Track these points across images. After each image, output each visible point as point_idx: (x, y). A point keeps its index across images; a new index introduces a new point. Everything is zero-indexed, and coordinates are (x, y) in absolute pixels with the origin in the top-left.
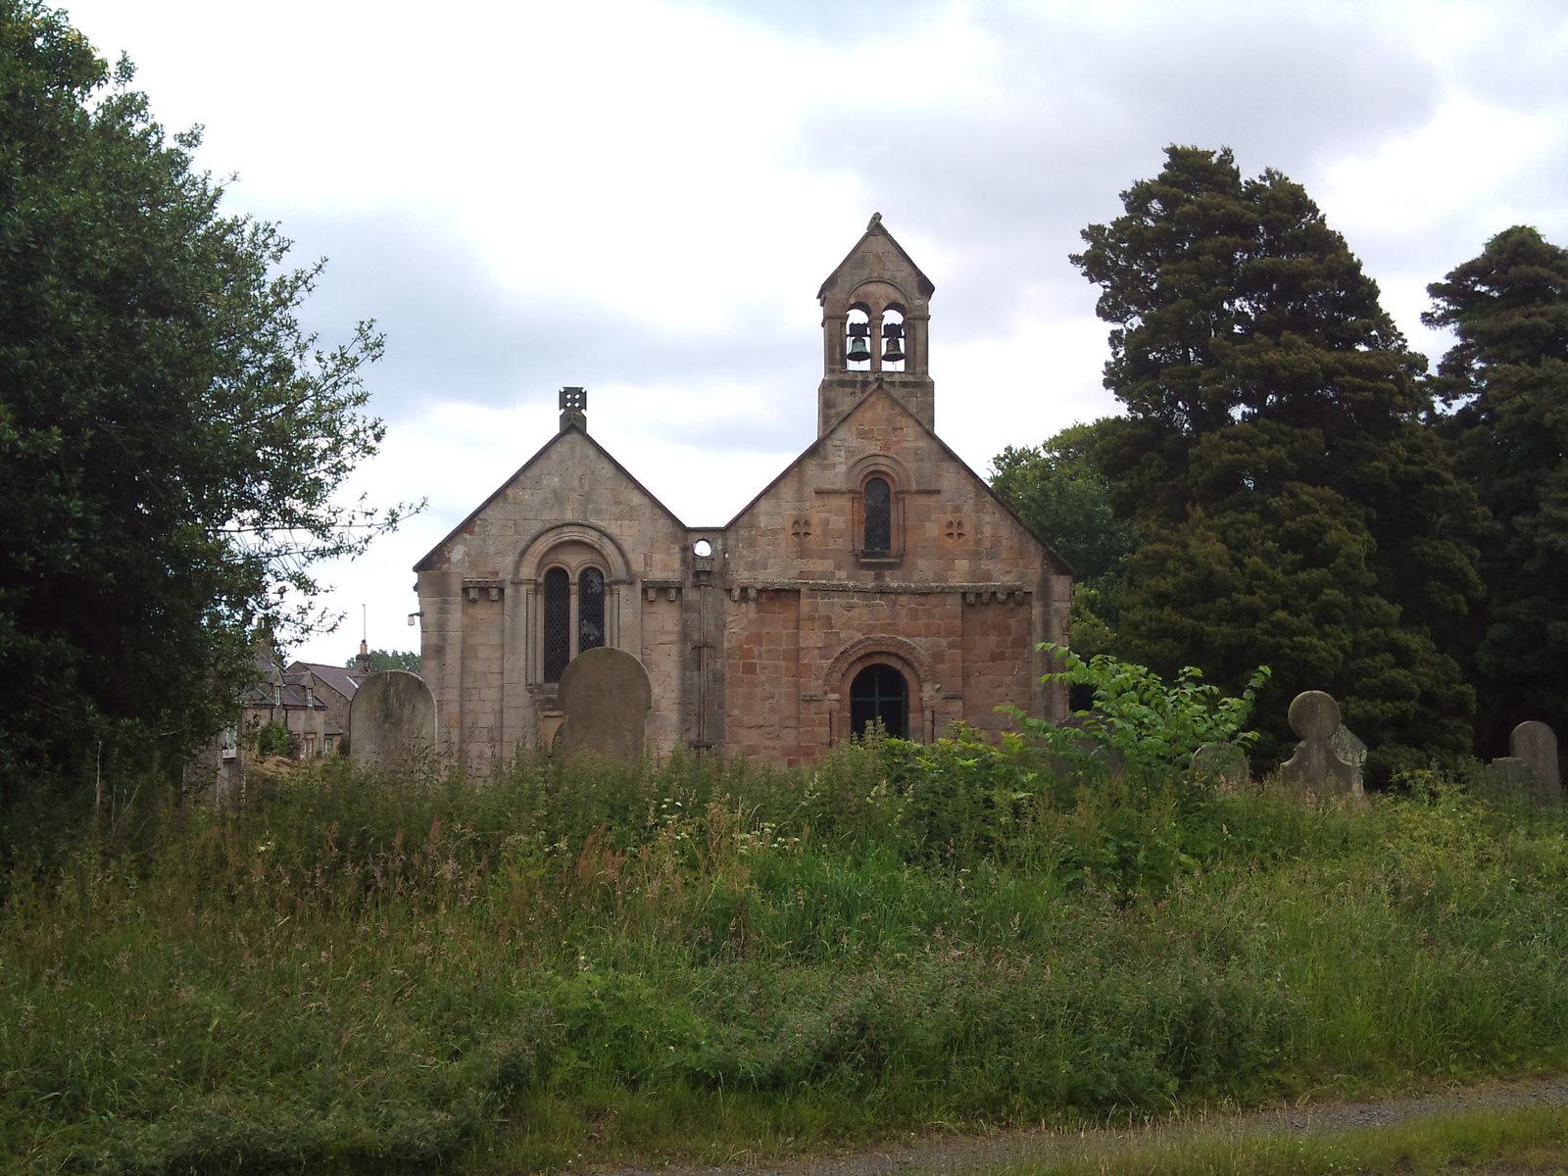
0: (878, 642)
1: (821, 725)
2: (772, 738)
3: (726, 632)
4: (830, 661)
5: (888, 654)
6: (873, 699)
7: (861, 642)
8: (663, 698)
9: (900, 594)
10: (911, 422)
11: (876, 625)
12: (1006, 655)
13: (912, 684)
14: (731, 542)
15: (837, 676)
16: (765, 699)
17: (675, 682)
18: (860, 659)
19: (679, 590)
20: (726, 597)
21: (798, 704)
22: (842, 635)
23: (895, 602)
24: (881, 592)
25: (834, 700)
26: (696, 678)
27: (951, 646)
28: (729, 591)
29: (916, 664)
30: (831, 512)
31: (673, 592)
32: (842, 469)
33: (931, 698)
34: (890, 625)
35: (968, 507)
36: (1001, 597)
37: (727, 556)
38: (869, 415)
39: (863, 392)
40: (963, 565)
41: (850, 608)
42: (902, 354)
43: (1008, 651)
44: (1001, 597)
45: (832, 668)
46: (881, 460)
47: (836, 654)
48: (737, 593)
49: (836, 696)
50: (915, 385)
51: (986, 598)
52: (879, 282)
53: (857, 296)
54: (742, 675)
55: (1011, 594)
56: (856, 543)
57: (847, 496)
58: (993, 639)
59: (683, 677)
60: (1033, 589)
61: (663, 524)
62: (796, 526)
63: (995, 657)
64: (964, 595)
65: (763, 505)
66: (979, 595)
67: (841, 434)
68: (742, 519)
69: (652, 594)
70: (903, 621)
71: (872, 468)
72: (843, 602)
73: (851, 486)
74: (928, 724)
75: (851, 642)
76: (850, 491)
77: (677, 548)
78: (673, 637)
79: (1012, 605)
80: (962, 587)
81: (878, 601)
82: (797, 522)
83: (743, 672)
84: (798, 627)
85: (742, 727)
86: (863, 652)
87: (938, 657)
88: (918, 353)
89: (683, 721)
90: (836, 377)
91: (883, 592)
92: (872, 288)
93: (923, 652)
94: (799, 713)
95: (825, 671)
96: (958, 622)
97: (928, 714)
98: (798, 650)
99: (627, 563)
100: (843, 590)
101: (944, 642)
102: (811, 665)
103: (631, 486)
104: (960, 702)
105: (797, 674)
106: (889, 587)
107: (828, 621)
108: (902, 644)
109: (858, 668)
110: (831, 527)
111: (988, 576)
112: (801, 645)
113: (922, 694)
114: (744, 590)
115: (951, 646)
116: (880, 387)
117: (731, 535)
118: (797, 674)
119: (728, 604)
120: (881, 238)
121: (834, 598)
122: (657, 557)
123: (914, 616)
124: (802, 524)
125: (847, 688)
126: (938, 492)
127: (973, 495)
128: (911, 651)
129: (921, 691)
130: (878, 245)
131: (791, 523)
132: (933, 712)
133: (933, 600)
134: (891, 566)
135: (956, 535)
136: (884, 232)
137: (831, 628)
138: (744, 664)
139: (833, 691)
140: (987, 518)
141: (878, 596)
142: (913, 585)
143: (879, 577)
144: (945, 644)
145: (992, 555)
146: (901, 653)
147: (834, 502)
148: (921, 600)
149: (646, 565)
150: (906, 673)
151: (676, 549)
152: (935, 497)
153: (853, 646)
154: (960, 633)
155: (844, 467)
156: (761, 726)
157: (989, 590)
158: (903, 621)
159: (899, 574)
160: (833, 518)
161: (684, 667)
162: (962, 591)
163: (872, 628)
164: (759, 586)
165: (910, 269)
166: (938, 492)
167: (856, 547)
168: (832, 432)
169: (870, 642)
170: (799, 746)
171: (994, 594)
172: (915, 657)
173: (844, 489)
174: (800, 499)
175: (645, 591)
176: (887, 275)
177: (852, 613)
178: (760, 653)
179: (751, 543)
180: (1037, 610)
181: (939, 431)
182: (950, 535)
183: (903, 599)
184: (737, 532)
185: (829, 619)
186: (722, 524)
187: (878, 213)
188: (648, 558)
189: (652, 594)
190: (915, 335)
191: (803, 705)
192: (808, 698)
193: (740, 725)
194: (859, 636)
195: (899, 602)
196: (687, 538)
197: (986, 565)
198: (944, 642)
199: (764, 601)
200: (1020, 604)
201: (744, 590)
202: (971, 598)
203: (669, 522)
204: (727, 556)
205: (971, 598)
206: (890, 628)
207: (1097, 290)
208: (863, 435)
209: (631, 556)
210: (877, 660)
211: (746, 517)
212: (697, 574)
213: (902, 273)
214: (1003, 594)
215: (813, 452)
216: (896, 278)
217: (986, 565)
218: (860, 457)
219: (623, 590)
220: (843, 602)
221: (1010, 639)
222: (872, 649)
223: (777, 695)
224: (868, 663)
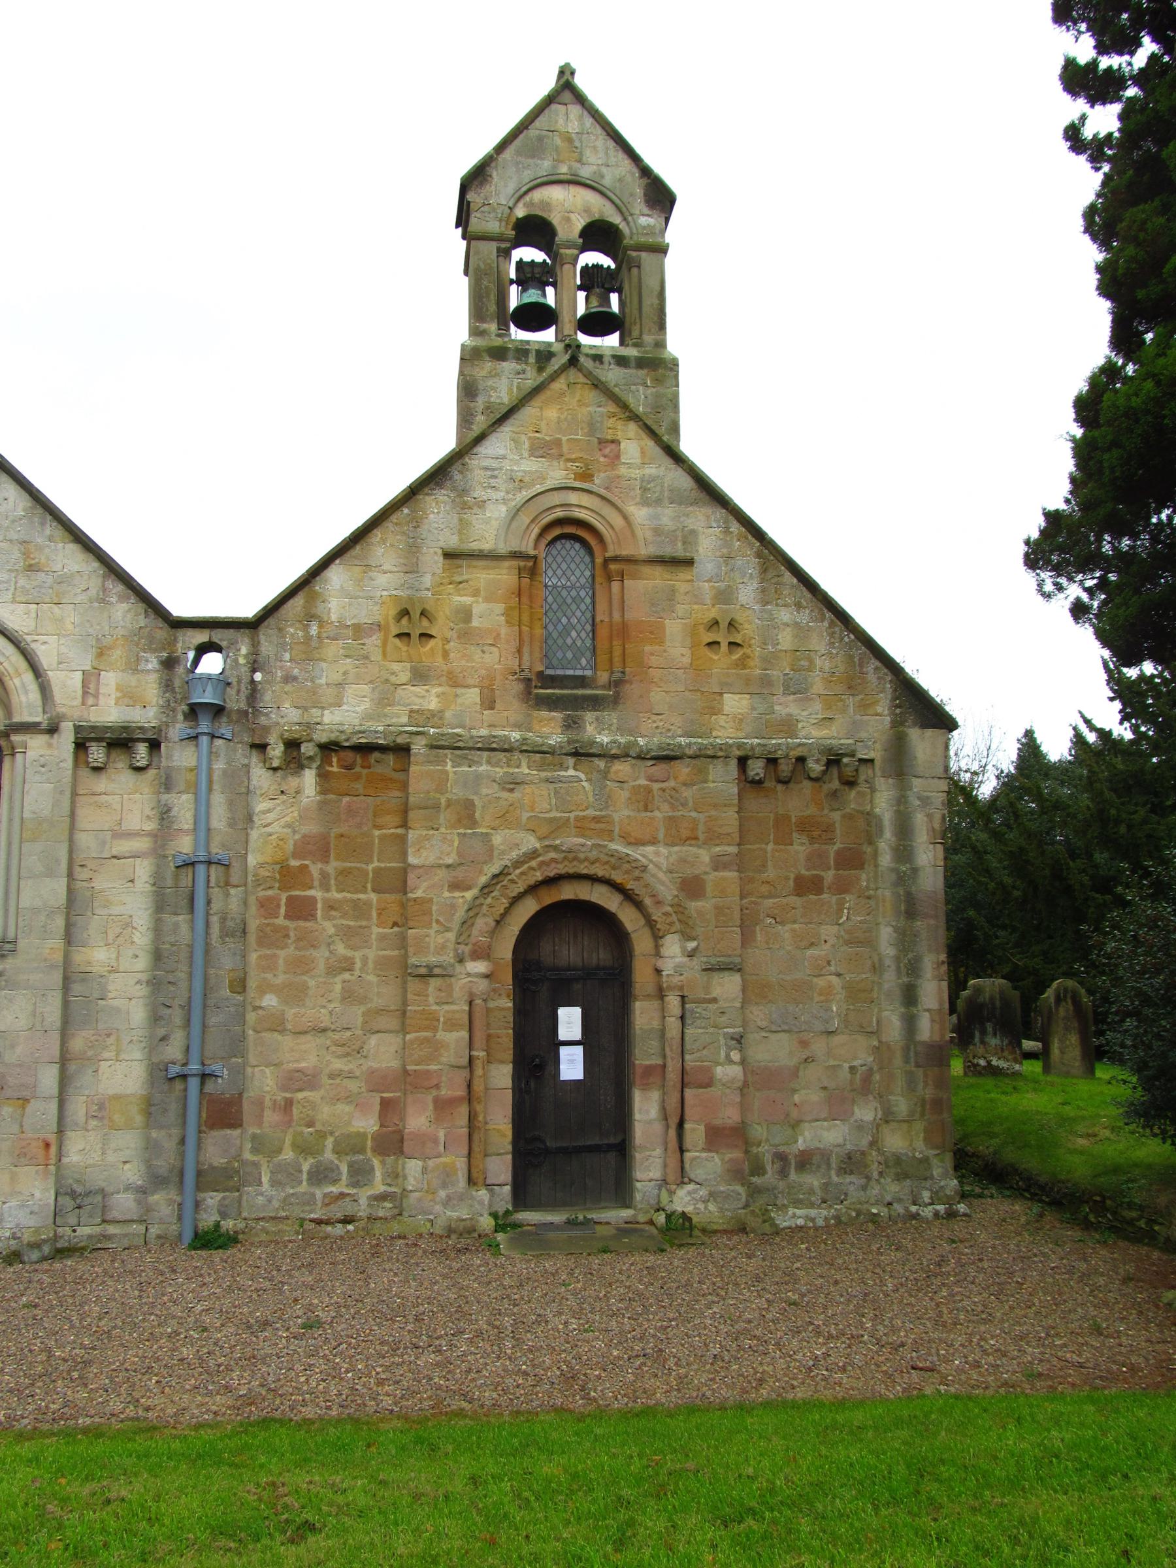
0: (571, 855)
1: (451, 1025)
2: (348, 1054)
3: (254, 834)
4: (469, 895)
5: (594, 879)
6: (319, 898)
7: (534, 854)
8: (113, 970)
9: (615, 757)
10: (632, 427)
11: (568, 819)
12: (826, 884)
13: (641, 943)
14: (267, 647)
15: (483, 923)
16: (332, 971)
17: (142, 938)
18: (533, 889)
19: (154, 745)
20: (255, 758)
21: (405, 982)
22: (497, 840)
23: (605, 774)
24: (576, 754)
25: (478, 975)
26: (184, 929)
27: (718, 864)
28: (261, 747)
29: (648, 901)
30: (476, 593)
31: (142, 749)
32: (497, 512)
33: (679, 970)
34: (596, 819)
35: (747, 593)
36: (815, 767)
37: (258, 676)
38: (552, 413)
39: (540, 369)
40: (735, 703)
41: (512, 784)
42: (612, 315)
43: (829, 876)
44: (815, 767)
45: (474, 909)
46: (573, 498)
47: (483, 880)
48: (277, 751)
49: (480, 967)
50: (641, 363)
51: (785, 768)
52: (569, 182)
53: (531, 204)
54: (287, 923)
55: (833, 760)
56: (526, 657)
57: (507, 564)
58: (800, 848)
59: (157, 929)
60: (875, 753)
61: (124, 612)
62: (404, 621)
63: (806, 886)
64: (743, 761)
65: (336, 576)
66: (772, 762)
67: (496, 446)
68: (291, 603)
69: (97, 753)
70: (622, 813)
71: (559, 513)
72: (499, 772)
73: (515, 545)
74: (673, 1024)
75: (514, 855)
76: (515, 555)
77: (155, 661)
78: (142, 844)
79: (836, 784)
80: (740, 746)
81: (571, 772)
82: (405, 613)
83: (285, 918)
84: (405, 825)
85: (282, 1032)
86: (539, 876)
87: (692, 887)
88: (646, 309)
89: (155, 1018)
90: (480, 342)
91: (581, 754)
92: (556, 194)
93: (661, 875)
94: (405, 1003)
95: (460, 914)
96: (730, 819)
97: (673, 1001)
98: (405, 871)
99: (45, 690)
100: (492, 748)
101: (705, 856)
102: (431, 900)
103: (59, 532)
104: (737, 978)
105: (402, 922)
106: (592, 743)
107: (466, 814)
108: (621, 860)
109: (529, 907)
110: (475, 623)
111: (788, 726)
112: (412, 860)
113: (660, 964)
114: (292, 745)
115: (718, 864)
116: (573, 361)
117: (267, 642)
118: (402, 922)
119: (260, 777)
120: (575, 110)
121: (479, 763)
122: (110, 680)
123: (644, 799)
124: (416, 614)
125: (505, 950)
126: (689, 563)
127: (756, 573)
128: (637, 873)
129: (658, 954)
130: (569, 119)
131: (393, 612)
132: (683, 997)
133: (683, 770)
134: (595, 703)
135: (724, 646)
136: (580, 99)
137: (473, 823)
138: (290, 900)
139: (476, 955)
140: (785, 615)
141: (571, 761)
142: (641, 741)
143: (571, 724)
144: (707, 859)
145: (796, 688)
146: (617, 877)
147: (482, 576)
148: (660, 769)
149: (85, 693)
150: (628, 918)
151: (152, 663)
152: (684, 574)
153: (517, 864)
154: (736, 836)
155: (504, 509)
156: (324, 1030)
157: (792, 754)
158: (622, 813)
159: (612, 717)
160: (479, 607)
161: (160, 904)
162: (738, 753)
163: (557, 826)
164: (323, 738)
165: (626, 164)
166: (689, 563)
167: (526, 664)
168: (480, 439)
169: (552, 855)
170: (406, 1072)
171: (801, 760)
172: (647, 886)
173: (503, 549)
174: (412, 568)
175: (81, 746)
176: (585, 172)
177: (516, 795)
178: (324, 876)
179: (309, 653)
180: (883, 802)
181: (688, 446)
182: (714, 644)
183: (621, 768)
184: (280, 630)
185: (469, 805)
186: (248, 609)
187: (567, 65)
188: (90, 682)
189: (97, 753)
190: (640, 279)
191: (413, 985)
192: (423, 971)
193: (277, 1025)
194: (531, 842)
195: (612, 776)
196: (175, 640)
197: (785, 706)
198: (705, 856)
199: (335, 769)
200: (851, 783)
201: (292, 745)
202: (756, 768)
203: (141, 607)
204: (258, 676)
205: (756, 768)
206: (593, 826)
207: (1069, 144)
208: (544, 449)
209: (55, 677)
210: (568, 892)
211: (298, 602)
212: (194, 712)
213: (618, 170)
214: (817, 761)
215: (437, 476)
216: (602, 177)
217: (785, 706)
218: (539, 488)
219: (36, 745)
220: (499, 772)
221: (832, 850)
222: (561, 869)
223: (358, 965)
224: (550, 897)
